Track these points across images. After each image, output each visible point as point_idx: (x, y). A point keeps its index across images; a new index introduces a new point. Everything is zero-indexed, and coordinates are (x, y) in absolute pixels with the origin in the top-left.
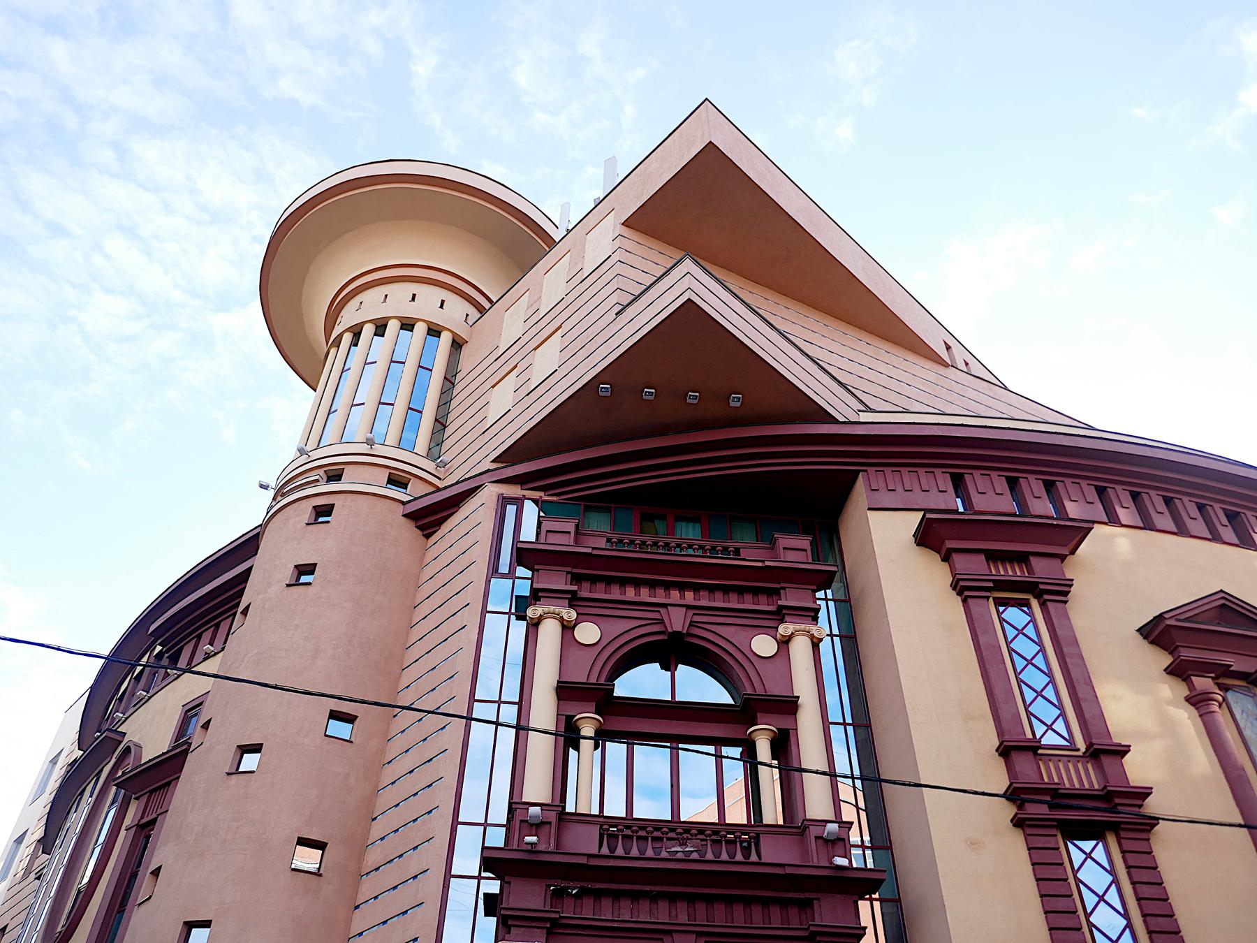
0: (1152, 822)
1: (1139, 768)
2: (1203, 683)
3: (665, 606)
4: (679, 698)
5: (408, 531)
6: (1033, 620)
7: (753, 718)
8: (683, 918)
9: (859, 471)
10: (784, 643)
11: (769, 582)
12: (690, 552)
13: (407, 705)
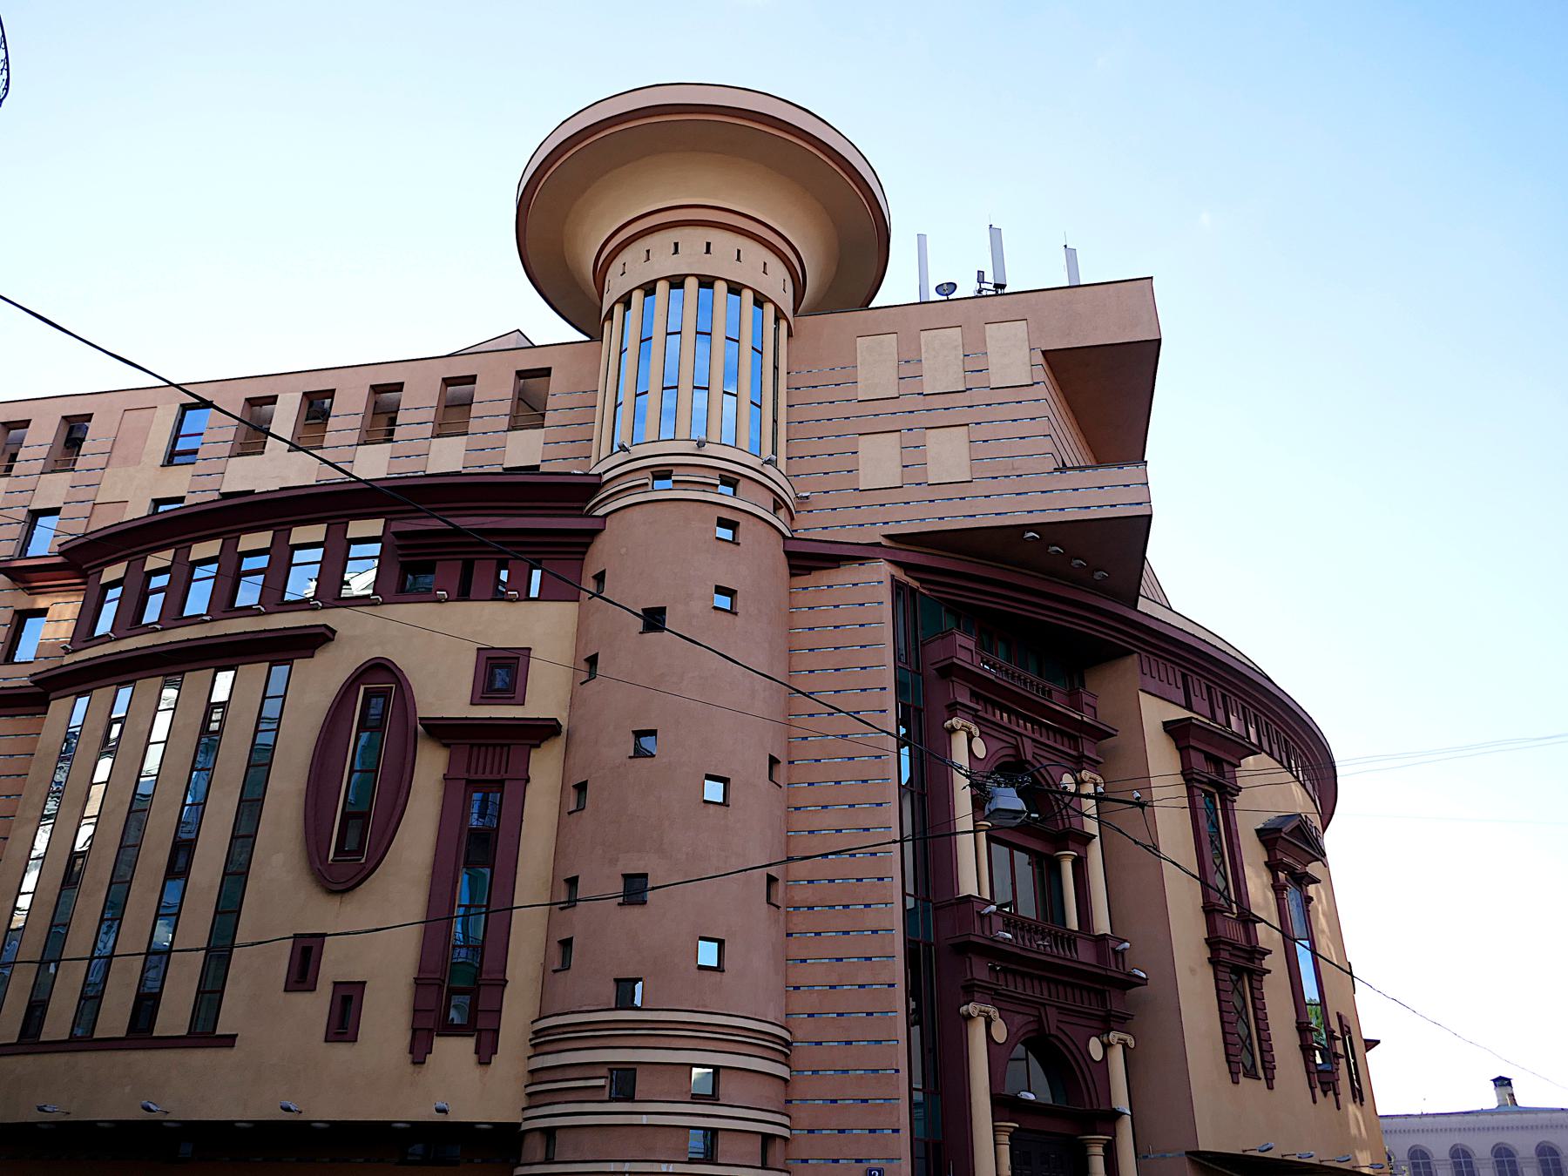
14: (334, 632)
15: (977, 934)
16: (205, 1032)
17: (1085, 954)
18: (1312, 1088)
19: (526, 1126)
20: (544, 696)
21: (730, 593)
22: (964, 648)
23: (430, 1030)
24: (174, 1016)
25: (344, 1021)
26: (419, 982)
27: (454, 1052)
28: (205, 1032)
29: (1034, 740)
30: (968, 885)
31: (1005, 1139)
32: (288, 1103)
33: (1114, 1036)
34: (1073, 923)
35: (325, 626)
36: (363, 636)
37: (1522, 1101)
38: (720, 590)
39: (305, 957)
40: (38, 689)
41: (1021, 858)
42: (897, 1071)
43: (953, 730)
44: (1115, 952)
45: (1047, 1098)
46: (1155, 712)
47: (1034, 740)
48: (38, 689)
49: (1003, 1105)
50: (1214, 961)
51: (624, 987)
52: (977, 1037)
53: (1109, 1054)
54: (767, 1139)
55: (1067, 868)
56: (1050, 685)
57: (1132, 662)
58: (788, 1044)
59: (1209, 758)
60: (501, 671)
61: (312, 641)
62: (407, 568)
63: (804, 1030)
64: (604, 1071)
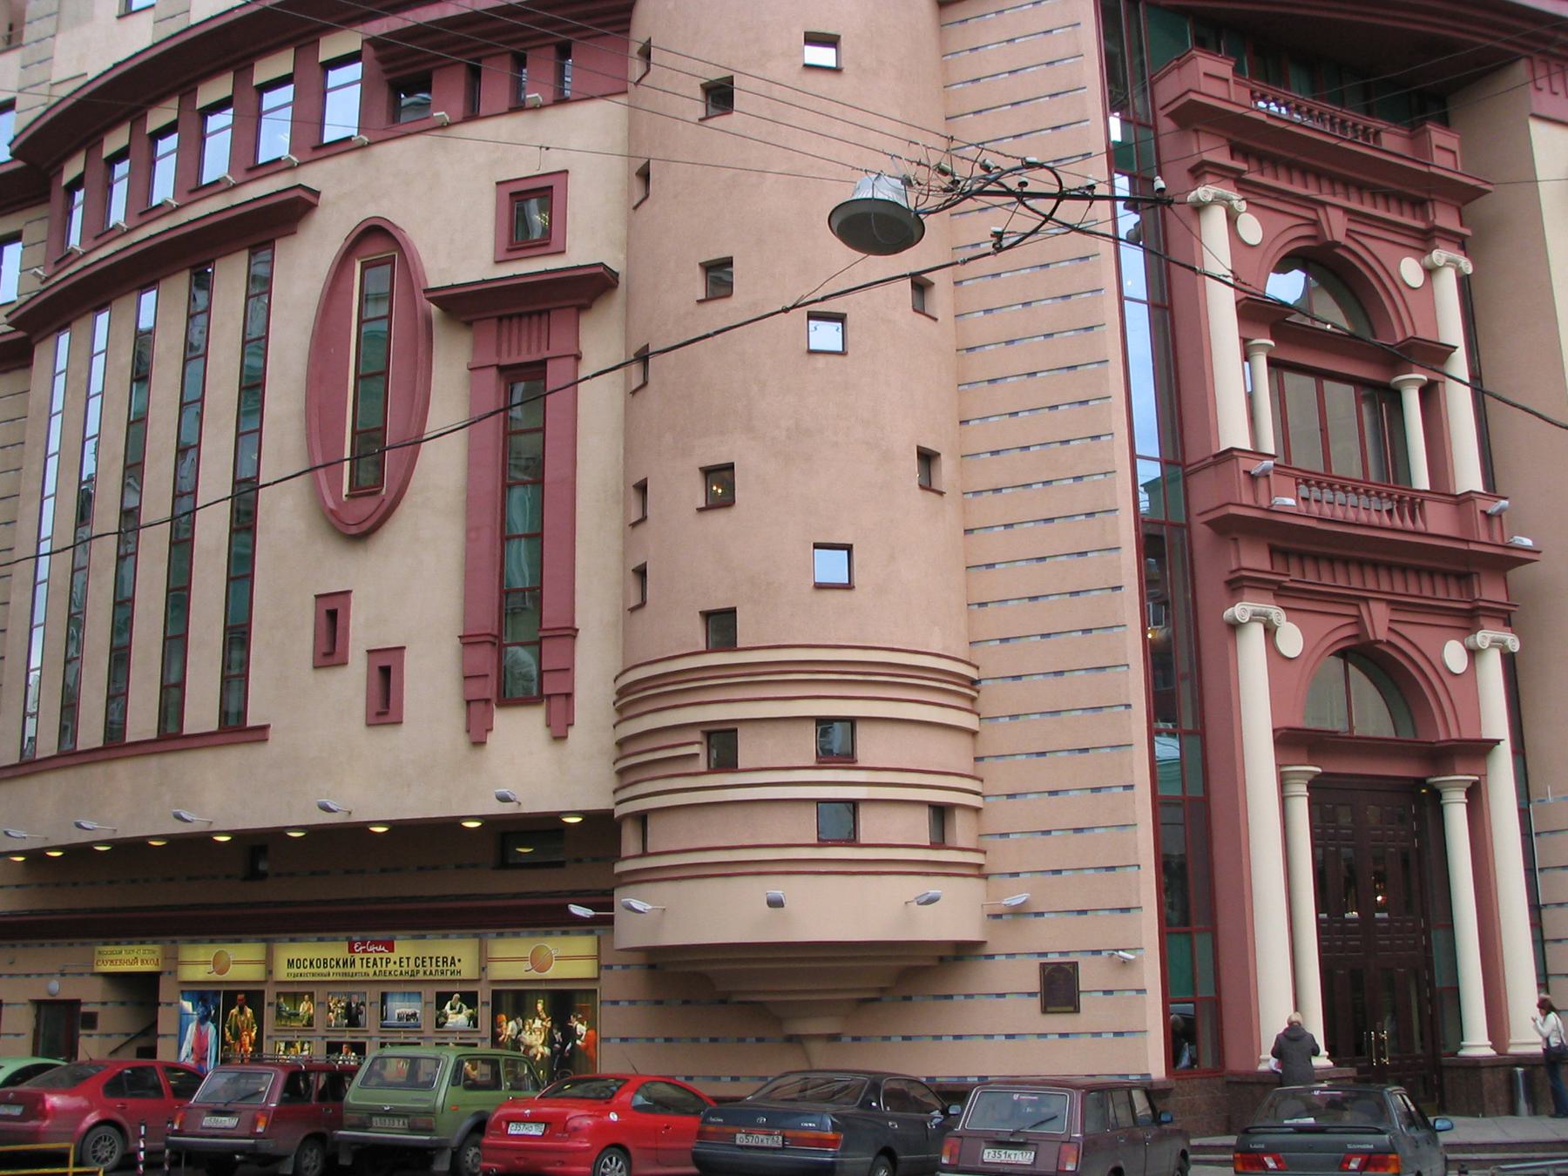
3: (1323, 204)
8: (1371, 585)
14: (317, 194)
15: (1244, 502)
16: (236, 727)
17: (1438, 520)
19: (619, 811)
20: (586, 241)
21: (830, 41)
22: (1210, 77)
23: (487, 701)
24: (201, 713)
25: (385, 702)
26: (468, 640)
27: (520, 728)
28: (236, 727)
29: (1346, 211)
30: (1233, 432)
31: (1300, 791)
33: (1483, 638)
34: (1422, 480)
35: (602, 264)
36: (346, 196)
37: (1334, 472)
38: (813, 39)
40: (20, 334)
41: (1341, 397)
42: (1128, 706)
44: (1488, 516)
45: (1387, 731)
47: (1346, 211)
48: (20, 334)
51: (721, 625)
52: (1252, 652)
54: (941, 813)
55: (1412, 399)
57: (1521, 69)
58: (973, 683)
60: (529, 206)
61: (291, 212)
62: (399, 87)
63: (994, 661)
64: (697, 736)
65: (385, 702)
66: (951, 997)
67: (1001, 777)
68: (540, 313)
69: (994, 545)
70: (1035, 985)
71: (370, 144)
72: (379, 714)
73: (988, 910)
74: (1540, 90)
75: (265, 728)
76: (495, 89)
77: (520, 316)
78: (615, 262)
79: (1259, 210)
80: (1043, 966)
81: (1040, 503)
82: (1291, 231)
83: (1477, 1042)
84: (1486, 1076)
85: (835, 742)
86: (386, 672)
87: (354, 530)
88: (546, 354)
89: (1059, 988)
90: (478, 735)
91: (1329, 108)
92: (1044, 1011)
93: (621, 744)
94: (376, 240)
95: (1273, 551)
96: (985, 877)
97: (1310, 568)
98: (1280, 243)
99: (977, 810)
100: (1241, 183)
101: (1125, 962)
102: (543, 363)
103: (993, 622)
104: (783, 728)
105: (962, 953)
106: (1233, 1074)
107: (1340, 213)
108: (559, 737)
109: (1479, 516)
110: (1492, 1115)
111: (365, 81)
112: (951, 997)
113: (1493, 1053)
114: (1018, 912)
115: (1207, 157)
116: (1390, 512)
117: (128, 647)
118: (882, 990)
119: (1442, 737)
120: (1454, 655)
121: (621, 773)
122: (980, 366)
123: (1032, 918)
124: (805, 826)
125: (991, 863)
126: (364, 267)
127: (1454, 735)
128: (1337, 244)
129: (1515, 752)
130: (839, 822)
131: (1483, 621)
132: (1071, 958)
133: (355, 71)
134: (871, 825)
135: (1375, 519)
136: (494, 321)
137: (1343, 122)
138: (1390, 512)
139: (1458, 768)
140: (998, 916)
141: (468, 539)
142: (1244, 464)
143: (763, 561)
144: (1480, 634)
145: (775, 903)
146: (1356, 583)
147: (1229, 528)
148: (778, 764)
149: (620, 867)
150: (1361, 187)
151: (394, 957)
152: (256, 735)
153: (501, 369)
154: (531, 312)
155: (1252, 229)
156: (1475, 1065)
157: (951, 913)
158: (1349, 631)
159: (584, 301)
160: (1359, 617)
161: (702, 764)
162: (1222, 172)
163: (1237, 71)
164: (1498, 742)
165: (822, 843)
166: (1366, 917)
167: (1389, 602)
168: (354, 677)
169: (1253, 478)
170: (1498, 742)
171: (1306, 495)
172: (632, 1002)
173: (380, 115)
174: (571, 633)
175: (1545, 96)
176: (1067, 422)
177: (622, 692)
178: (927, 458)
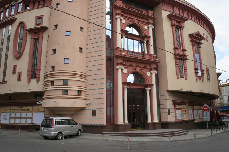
0: (186, 59)
1: (187, 53)
2: (194, 44)
3: (134, 19)
4: (134, 33)
5: (53, 66)
6: (179, 32)
7: (142, 38)
8: (137, 65)
9: (161, 2)
10: (148, 28)
11: (147, 18)
12: (134, 9)
13: (92, 22)
14: (16, 18)
17: (147, 57)
18: (197, 79)
20: (45, 24)
25: (19, 79)
26: (28, 71)
27: (33, 81)
29: (137, 20)
32: (30, 88)
33: (152, 72)
39: (15, 68)
43: (116, 19)
46: (165, 14)
47: (137, 20)
49: (125, 83)
50: (175, 58)
51: (53, 68)
53: (151, 76)
56: (142, 10)
57: (161, 4)
59: (177, 21)
60: (39, 18)
63: (89, 73)
64: (50, 82)
65: (19, 79)
66: (82, 114)
67: (89, 87)
68: (39, 32)
69: (89, 59)
70: (91, 113)
71: (22, 12)
72: (19, 80)
73: (86, 103)
74: (163, 6)
75: (7, 81)
76: (36, 6)
77: (37, 32)
78: (47, 26)
79: (125, 19)
80: (92, 110)
81: (95, 54)
82: (130, 22)
83: (149, 121)
84: (149, 125)
85: (66, 82)
86: (20, 74)
87: (17, 58)
88: (39, 37)
89: (94, 113)
90: (29, 82)
91: (137, 8)
92: (92, 116)
93: (44, 82)
94: (22, 24)
95: (123, 60)
96: (86, 99)
97: (141, 64)
98: (128, 23)
99: (86, 91)
100: (122, 16)
101: (101, 110)
102: (39, 38)
103: (89, 69)
104: (59, 81)
105: (83, 109)
106: (115, 124)
107: (136, 20)
108: (38, 82)
109: (119, 51)
110: (150, 130)
111: (22, 5)
112: (82, 114)
113: (151, 122)
114: (90, 104)
115: (117, 12)
116: (142, 56)
117: (6, 72)
118: (74, 113)
119: (147, 83)
120: (149, 74)
121: (44, 86)
122: (90, 38)
123: (91, 105)
124: (61, 93)
125: (87, 98)
126: (21, 27)
127: (148, 83)
128: (136, 24)
129: (156, 86)
130: (65, 92)
131: (152, 70)
132: (95, 110)
133: (21, 4)
134: (69, 93)
135: (140, 57)
136: (34, 33)
137: (138, 9)
138: (142, 56)
139: (148, 87)
140: (87, 104)
141: (29, 59)
142: (119, 49)
143: (57, 60)
144: (152, 71)
145: (55, 102)
146: (145, 66)
147: (118, 57)
148: (59, 85)
149: (43, 97)
150: (140, 17)
151: (23, 109)
152: (6, 82)
153: (34, 39)
154: (39, 31)
155: (124, 21)
156: (148, 124)
157: (80, 103)
158: (134, 70)
159: (44, 31)
160: (135, 69)
161: (50, 85)
162: (119, 14)
163: (122, 2)
164: (153, 84)
165: (63, 95)
166: (136, 106)
167: (139, 67)
168: (16, 76)
169: (154, 57)
170: (153, 84)
171: (132, 54)
172: (48, 114)
173: (24, 9)
174: (40, 70)
175: (164, 7)
176: (98, 44)
177: (45, 76)
178: (81, 49)
